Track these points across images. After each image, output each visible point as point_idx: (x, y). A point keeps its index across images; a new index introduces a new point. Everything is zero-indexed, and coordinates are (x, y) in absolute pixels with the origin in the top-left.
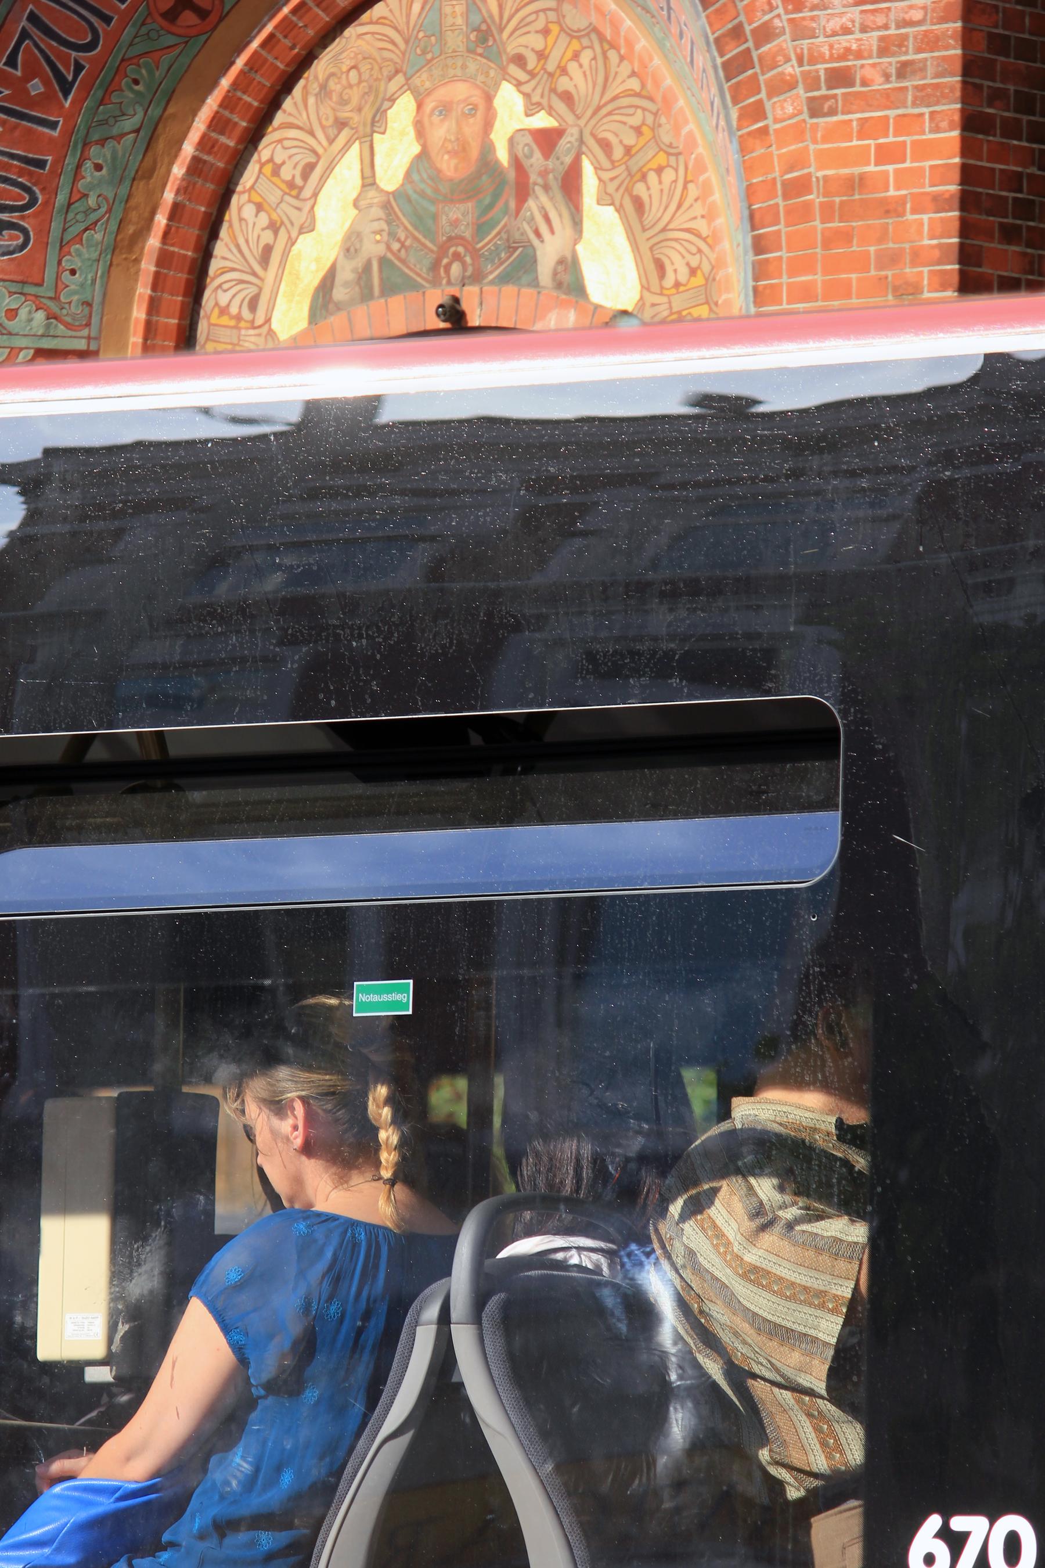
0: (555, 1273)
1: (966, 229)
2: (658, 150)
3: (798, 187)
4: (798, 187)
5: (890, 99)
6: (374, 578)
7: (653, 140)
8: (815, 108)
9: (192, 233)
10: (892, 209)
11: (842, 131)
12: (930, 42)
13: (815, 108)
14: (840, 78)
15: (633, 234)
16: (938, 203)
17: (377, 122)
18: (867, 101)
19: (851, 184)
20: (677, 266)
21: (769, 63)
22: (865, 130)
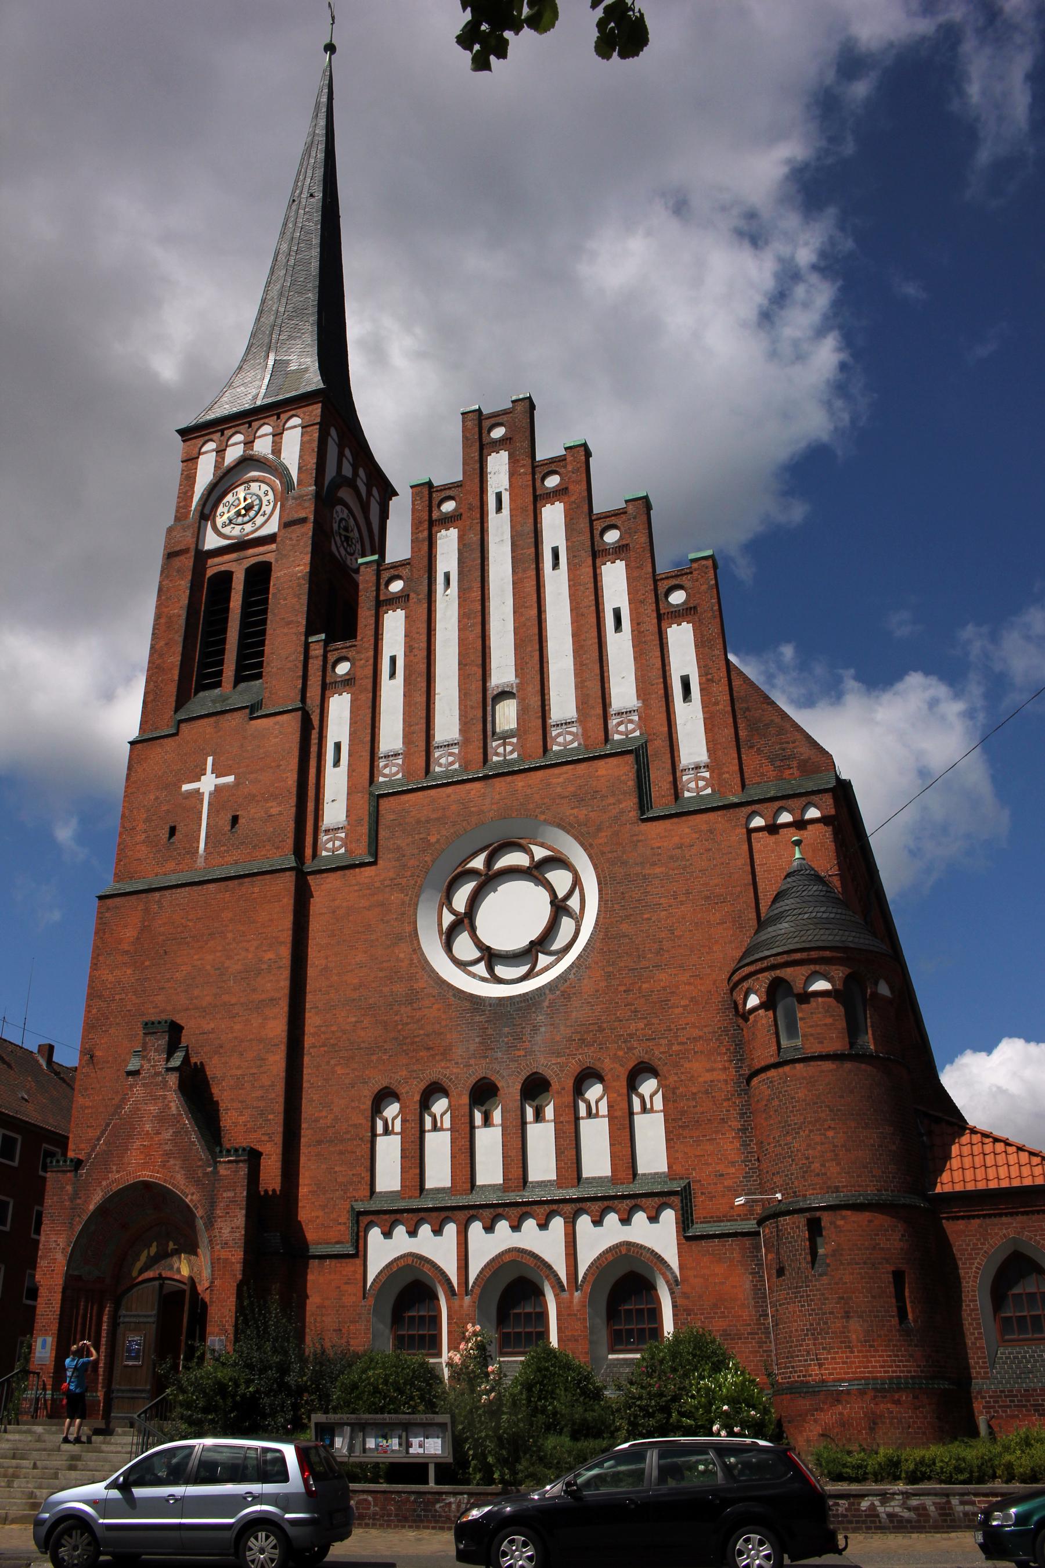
0: (186, 1308)
1: (244, 1267)
2: (595, 523)
3: (219, 1259)
4: (219, 1259)
5: (233, 1247)
6: (371, 1037)
7: (375, 567)
8: (222, 1248)
9: (572, 1248)
10: (233, 1263)
11: (226, 1251)
12: (240, 1239)
13: (222, 1248)
14: (226, 1244)
15: (559, 461)
16: (240, 1263)
17: (151, 1246)
18: (229, 1247)
19: (227, 1259)
20: (195, 1269)
21: (216, 1241)
22: (230, 1251)
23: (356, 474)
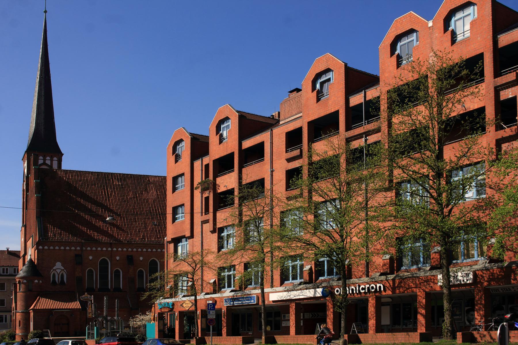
23: (45, 160)
